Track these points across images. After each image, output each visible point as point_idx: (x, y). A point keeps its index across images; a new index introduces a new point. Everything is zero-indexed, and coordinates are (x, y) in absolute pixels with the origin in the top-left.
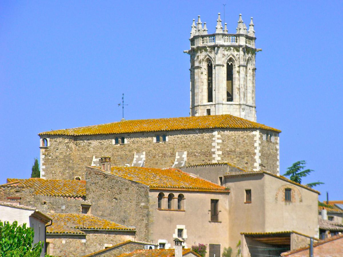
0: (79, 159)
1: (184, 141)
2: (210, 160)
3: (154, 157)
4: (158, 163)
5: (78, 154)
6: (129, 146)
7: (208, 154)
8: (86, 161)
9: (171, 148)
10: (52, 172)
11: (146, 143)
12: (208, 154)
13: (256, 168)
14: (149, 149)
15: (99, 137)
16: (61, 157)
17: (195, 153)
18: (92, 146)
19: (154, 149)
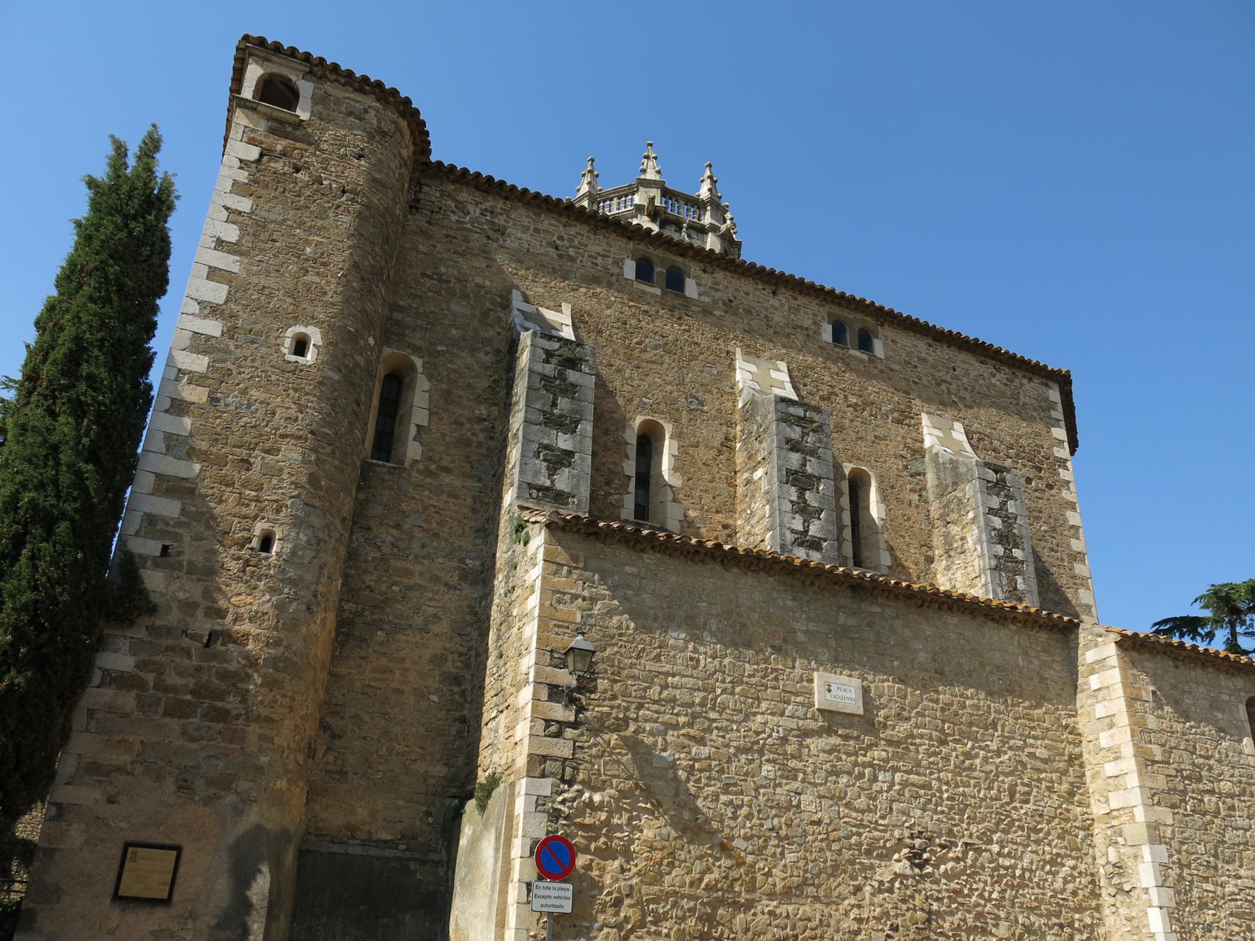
0: (423, 275)
8: (465, 296)
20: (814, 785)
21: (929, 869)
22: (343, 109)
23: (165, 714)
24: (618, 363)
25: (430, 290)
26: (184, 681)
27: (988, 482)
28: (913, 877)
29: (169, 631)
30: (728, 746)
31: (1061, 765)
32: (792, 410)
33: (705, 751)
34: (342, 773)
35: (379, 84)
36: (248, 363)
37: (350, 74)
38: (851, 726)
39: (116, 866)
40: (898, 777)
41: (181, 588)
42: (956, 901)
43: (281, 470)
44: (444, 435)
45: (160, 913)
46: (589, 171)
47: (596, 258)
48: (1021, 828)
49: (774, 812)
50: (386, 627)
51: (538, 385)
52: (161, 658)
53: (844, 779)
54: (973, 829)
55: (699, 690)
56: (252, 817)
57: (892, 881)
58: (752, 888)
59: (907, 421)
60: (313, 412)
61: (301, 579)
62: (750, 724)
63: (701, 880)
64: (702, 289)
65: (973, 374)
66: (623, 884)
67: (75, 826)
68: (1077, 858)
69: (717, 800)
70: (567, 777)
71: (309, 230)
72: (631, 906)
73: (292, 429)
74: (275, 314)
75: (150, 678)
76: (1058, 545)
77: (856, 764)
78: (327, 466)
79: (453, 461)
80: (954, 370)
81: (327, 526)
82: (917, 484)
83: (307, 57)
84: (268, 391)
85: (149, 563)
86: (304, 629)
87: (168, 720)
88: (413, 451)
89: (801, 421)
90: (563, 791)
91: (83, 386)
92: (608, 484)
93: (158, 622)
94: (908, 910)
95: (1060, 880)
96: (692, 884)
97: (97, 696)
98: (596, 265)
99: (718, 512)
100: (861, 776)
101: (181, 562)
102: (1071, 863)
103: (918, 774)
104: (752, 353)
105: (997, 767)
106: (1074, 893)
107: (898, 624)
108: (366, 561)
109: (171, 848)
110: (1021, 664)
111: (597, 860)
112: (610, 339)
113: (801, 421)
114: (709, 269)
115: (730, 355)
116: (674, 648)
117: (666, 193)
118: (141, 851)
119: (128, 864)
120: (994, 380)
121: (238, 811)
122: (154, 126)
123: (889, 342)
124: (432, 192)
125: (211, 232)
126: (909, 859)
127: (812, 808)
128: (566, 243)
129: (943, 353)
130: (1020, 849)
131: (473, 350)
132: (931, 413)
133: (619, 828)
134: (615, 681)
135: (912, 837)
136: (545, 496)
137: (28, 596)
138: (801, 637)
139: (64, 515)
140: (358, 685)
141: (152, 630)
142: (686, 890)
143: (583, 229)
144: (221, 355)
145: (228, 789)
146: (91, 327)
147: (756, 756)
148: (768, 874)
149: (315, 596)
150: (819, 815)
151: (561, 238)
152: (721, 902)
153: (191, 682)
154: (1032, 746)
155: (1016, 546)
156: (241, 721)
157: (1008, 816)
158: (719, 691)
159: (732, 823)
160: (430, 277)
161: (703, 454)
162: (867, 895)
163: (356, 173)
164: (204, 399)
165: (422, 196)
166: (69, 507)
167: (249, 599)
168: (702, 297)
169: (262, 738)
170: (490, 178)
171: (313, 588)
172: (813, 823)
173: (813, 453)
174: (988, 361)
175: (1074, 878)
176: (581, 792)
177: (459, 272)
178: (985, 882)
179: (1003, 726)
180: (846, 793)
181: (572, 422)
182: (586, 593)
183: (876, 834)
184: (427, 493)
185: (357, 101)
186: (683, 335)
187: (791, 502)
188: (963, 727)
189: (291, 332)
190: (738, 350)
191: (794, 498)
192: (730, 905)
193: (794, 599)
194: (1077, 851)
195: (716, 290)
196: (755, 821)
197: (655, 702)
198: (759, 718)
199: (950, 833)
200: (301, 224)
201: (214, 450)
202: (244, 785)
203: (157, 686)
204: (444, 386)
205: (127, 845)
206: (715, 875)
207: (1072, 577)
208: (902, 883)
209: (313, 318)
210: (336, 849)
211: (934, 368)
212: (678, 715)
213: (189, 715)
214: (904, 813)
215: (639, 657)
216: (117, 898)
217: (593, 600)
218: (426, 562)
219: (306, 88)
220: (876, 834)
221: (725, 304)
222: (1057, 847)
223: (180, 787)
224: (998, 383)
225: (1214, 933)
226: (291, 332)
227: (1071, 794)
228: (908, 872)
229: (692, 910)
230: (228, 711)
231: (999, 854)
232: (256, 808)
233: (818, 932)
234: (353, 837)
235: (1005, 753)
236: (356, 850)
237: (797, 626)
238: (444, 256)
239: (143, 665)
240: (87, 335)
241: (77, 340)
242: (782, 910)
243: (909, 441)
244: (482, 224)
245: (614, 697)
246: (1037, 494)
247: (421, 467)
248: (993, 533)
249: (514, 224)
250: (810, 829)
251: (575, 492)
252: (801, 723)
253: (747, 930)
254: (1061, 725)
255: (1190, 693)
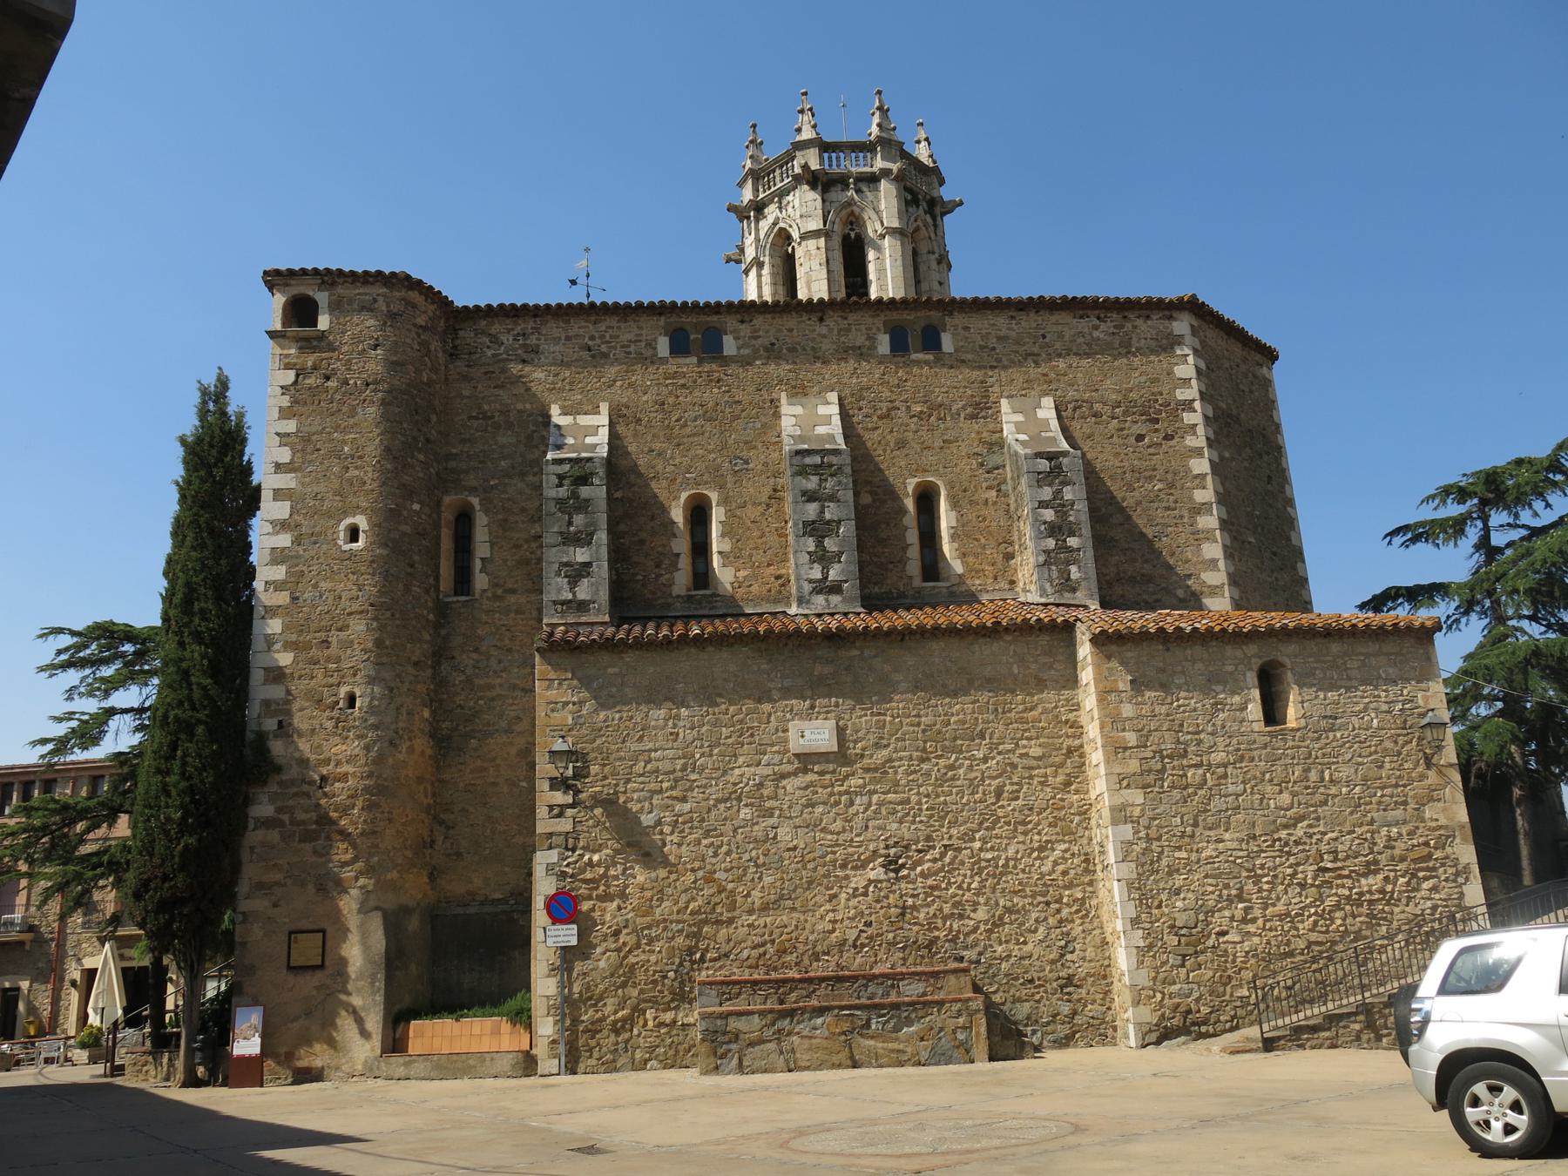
0: (470, 418)
5: (466, 393)
8: (510, 426)
15: (583, 324)
20: (791, 818)
21: (904, 872)
22: (356, 306)
23: (300, 841)
24: (657, 446)
25: (477, 430)
26: (309, 816)
27: (1039, 473)
28: (888, 881)
29: (293, 782)
30: (708, 799)
31: (1057, 759)
32: (808, 460)
33: (687, 807)
34: (458, 854)
35: (379, 273)
36: (315, 561)
37: (353, 273)
38: (828, 762)
39: (286, 948)
40: (875, 798)
42: (932, 895)
43: (352, 642)
45: (319, 974)
46: (751, 142)
48: (1008, 823)
49: (751, 846)
50: (477, 735)
51: (554, 510)
52: (291, 803)
53: (819, 809)
54: (954, 831)
55: (679, 758)
57: (866, 887)
58: (732, 907)
59: (983, 414)
60: (371, 585)
61: (381, 722)
62: (728, 778)
63: (687, 907)
64: (741, 342)
65: (1068, 334)
66: (620, 919)
68: (1070, 842)
69: (699, 844)
70: (570, 846)
71: (344, 431)
72: (628, 934)
73: (356, 607)
74: (328, 514)
75: (286, 818)
76: (1176, 502)
77: (832, 794)
78: (389, 628)
80: (1044, 337)
81: (398, 676)
82: (995, 479)
83: (316, 271)
84: (333, 580)
85: (271, 736)
86: (391, 761)
88: (480, 581)
89: (817, 469)
90: (568, 857)
91: (197, 620)
92: (658, 566)
93: (284, 778)
94: (882, 908)
95: (1050, 864)
96: (678, 912)
97: (254, 837)
98: (629, 353)
99: (769, 565)
100: (837, 803)
102: (1063, 846)
103: (896, 792)
104: (799, 392)
105: (983, 773)
106: (1064, 873)
108: (454, 685)
109: (318, 931)
110: (1016, 671)
111: (599, 904)
112: (649, 425)
113: (817, 469)
114: (747, 318)
115: (775, 404)
116: (655, 728)
117: (825, 147)
118: (300, 936)
119: (293, 946)
120: (1096, 334)
122: (220, 368)
124: (467, 335)
125: (270, 459)
126: (883, 866)
127: (788, 838)
128: (598, 341)
129: (1029, 321)
130: (1005, 841)
132: (1012, 397)
133: (616, 878)
134: (605, 765)
135: (887, 847)
136: (568, 608)
137: (183, 784)
139: (199, 722)
140: (461, 785)
141: (281, 784)
142: (675, 917)
143: (612, 321)
144: (295, 561)
146: (195, 570)
147: (734, 803)
148: (748, 895)
149: (397, 733)
150: (795, 842)
151: (592, 338)
152: (706, 922)
153: (313, 815)
154: (1025, 747)
155: (1072, 534)
157: (992, 815)
158: (698, 756)
159: (714, 860)
160: (476, 418)
161: (752, 512)
162: (843, 901)
163: (374, 364)
164: (288, 600)
165: (458, 342)
166: (201, 716)
167: (344, 747)
170: (513, 306)
171: (393, 727)
172: (789, 850)
174: (1089, 312)
175: (1066, 860)
176: (582, 856)
178: (965, 876)
179: (992, 734)
180: (821, 820)
181: (587, 535)
182: (575, 699)
183: (851, 850)
184: (497, 615)
185: (366, 294)
186: (723, 397)
187: (809, 553)
188: (947, 743)
189: (342, 526)
190: (783, 395)
191: (812, 548)
192: (713, 923)
193: (770, 661)
194: (1069, 834)
196: (734, 856)
197: (641, 775)
198: (737, 772)
199: (928, 838)
200: (337, 428)
201: (301, 639)
203: (292, 823)
204: (500, 517)
205: (290, 933)
206: (700, 902)
207: (1193, 534)
208: (876, 887)
209: (358, 507)
210: (460, 911)
212: (661, 782)
213: (316, 839)
214: (879, 828)
215: (623, 742)
216: (290, 968)
217: (581, 703)
218: (504, 675)
219: (322, 298)
220: (851, 850)
221: (766, 350)
222: (1048, 833)
223: (319, 890)
224: (1102, 336)
225: (1182, 896)
226: (342, 526)
227: (1068, 784)
228: (883, 877)
229: (681, 931)
231: (981, 849)
233: (794, 935)
234: (474, 900)
235: (993, 758)
236: (472, 910)
237: (772, 685)
239: (279, 810)
240: (194, 579)
241: (188, 584)
242: (761, 921)
243: (984, 435)
244: (516, 350)
245: (605, 778)
246: (1151, 450)
247: (489, 594)
248: (1043, 528)
250: (787, 855)
251: (595, 597)
252: (777, 768)
253: (730, 940)
254: (1061, 722)
255: (1183, 672)
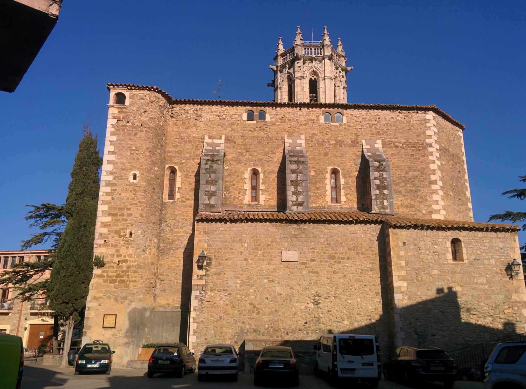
0: (176, 138)
1: (376, 125)
2: (424, 156)
3: (321, 145)
4: (329, 154)
6: (273, 124)
7: (419, 147)
8: (190, 142)
9: (352, 134)
10: (131, 147)
11: (305, 123)
12: (419, 147)
13: (438, 212)
14: (311, 132)
16: (151, 125)
17: (397, 144)
18: (203, 120)
19: (321, 132)
22: (139, 98)
23: (110, 283)
26: (113, 274)
41: (110, 251)
44: (187, 189)
45: (113, 330)
47: (233, 116)
50: (173, 249)
52: (107, 269)
56: (133, 305)
65: (388, 118)
67: (92, 312)
75: (105, 274)
78: (145, 210)
79: (190, 196)
87: (110, 284)
101: (109, 244)
107: (314, 231)
118: (107, 316)
121: (129, 304)
123: (349, 115)
128: (222, 114)
131: (194, 159)
138: (278, 240)
140: (167, 266)
145: (126, 300)
153: (115, 274)
156: (128, 282)
160: (179, 139)
168: (272, 119)
169: (134, 286)
173: (301, 173)
177: (187, 134)
184: (183, 207)
191: (293, 190)
195: (277, 115)
202: (130, 298)
204: (185, 173)
205: (104, 315)
211: (369, 120)
216: (103, 327)
221: (280, 119)
224: (400, 119)
230: (124, 280)
232: (134, 303)
234: (169, 307)
238: (182, 130)
247: (180, 200)
249: (204, 112)
